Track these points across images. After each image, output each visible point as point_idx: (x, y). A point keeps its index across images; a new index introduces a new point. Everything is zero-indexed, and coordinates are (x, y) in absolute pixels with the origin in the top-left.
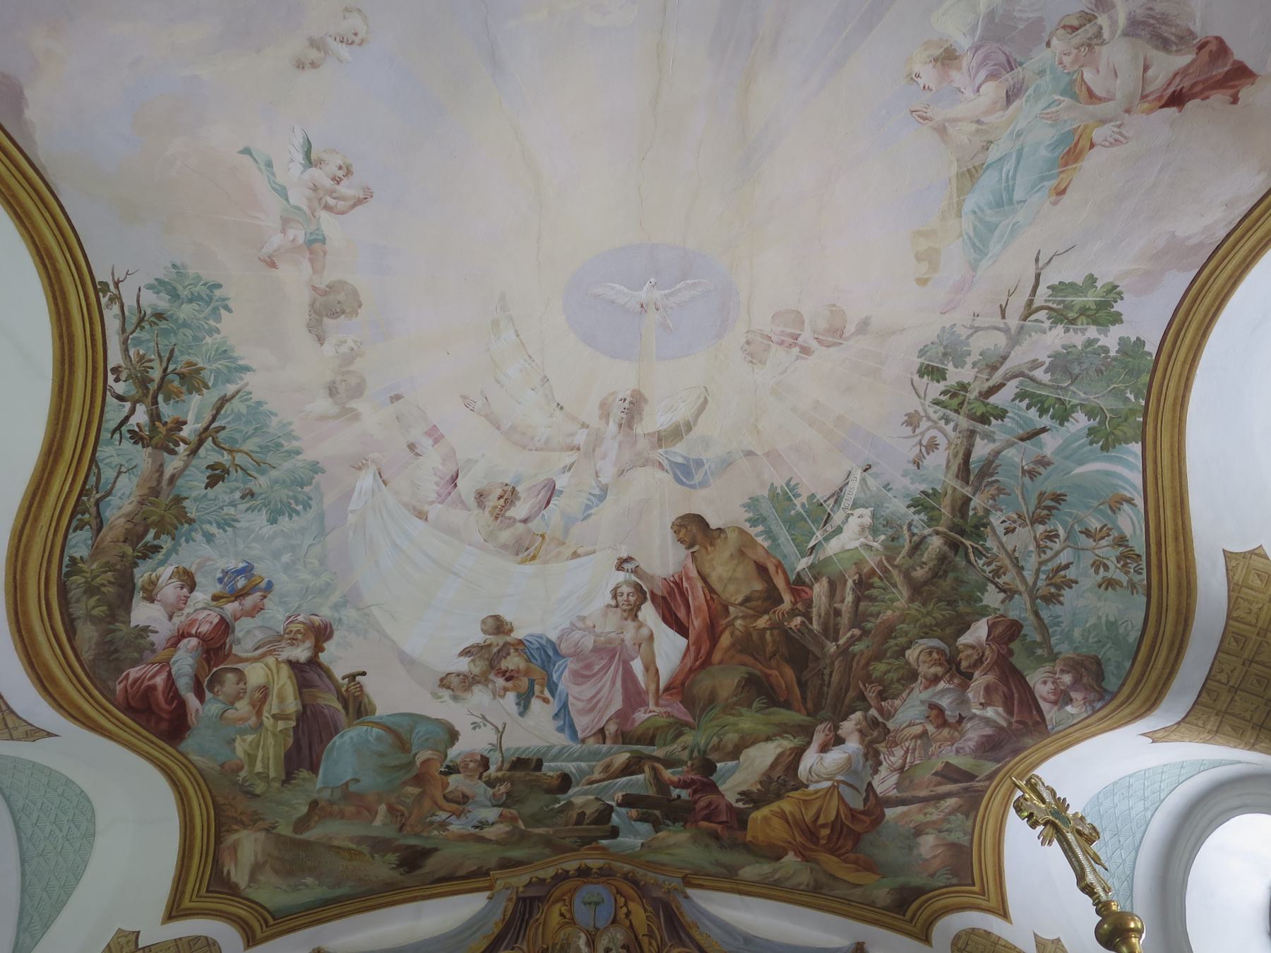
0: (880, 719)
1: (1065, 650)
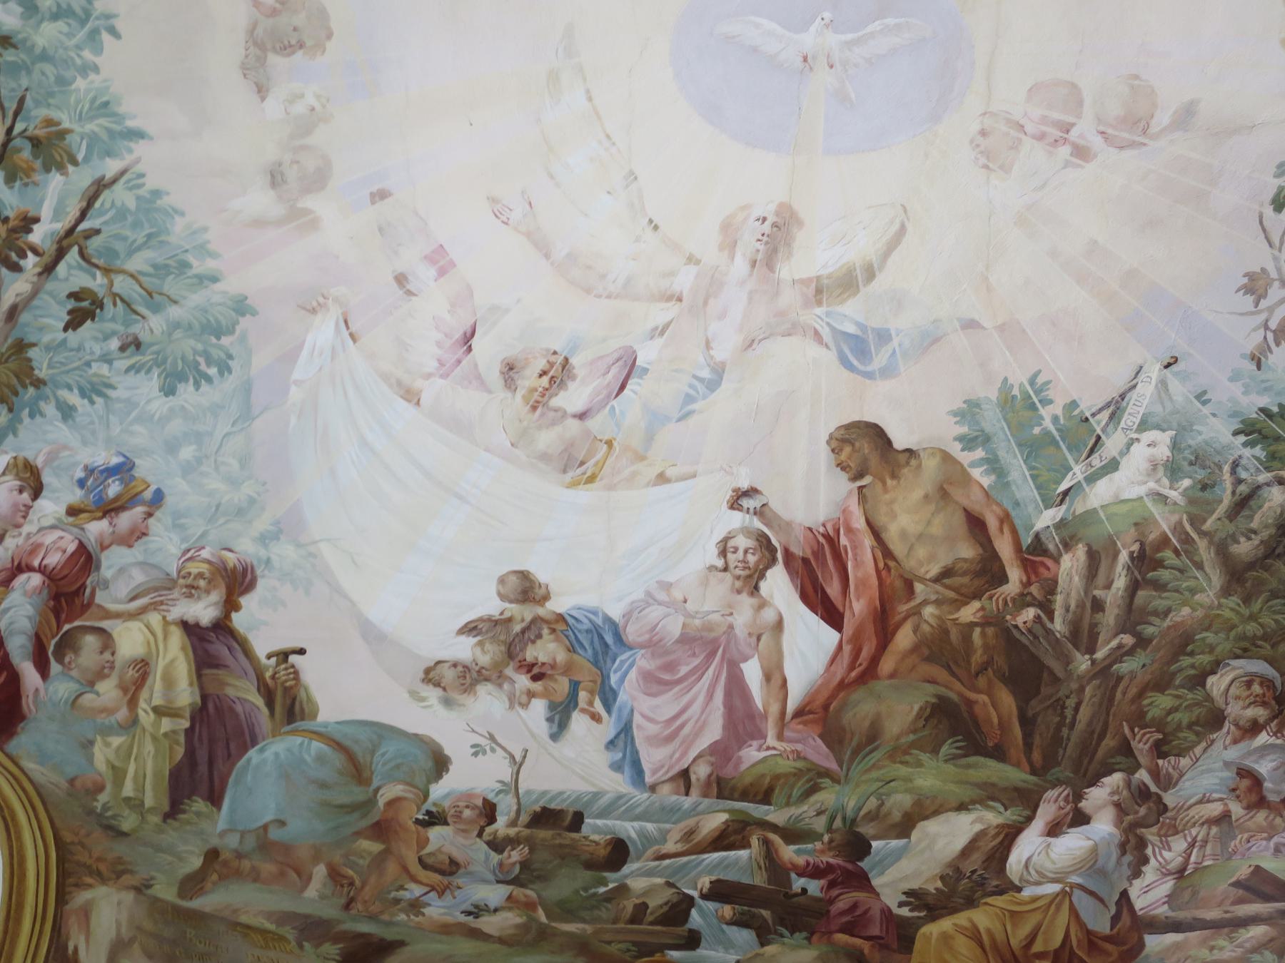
0: (1153, 788)
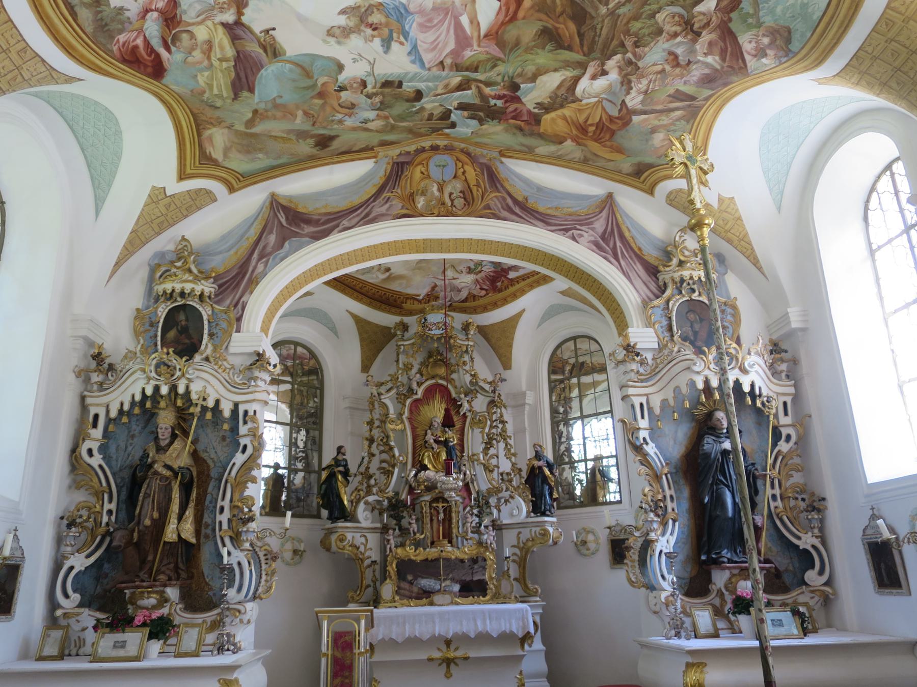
0: (634, 60)
1: (768, 21)
